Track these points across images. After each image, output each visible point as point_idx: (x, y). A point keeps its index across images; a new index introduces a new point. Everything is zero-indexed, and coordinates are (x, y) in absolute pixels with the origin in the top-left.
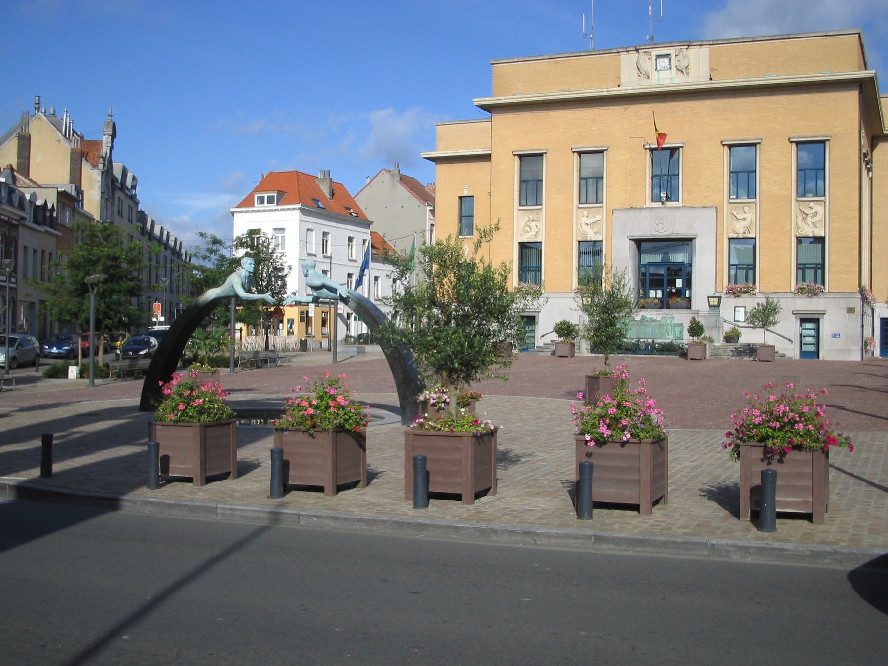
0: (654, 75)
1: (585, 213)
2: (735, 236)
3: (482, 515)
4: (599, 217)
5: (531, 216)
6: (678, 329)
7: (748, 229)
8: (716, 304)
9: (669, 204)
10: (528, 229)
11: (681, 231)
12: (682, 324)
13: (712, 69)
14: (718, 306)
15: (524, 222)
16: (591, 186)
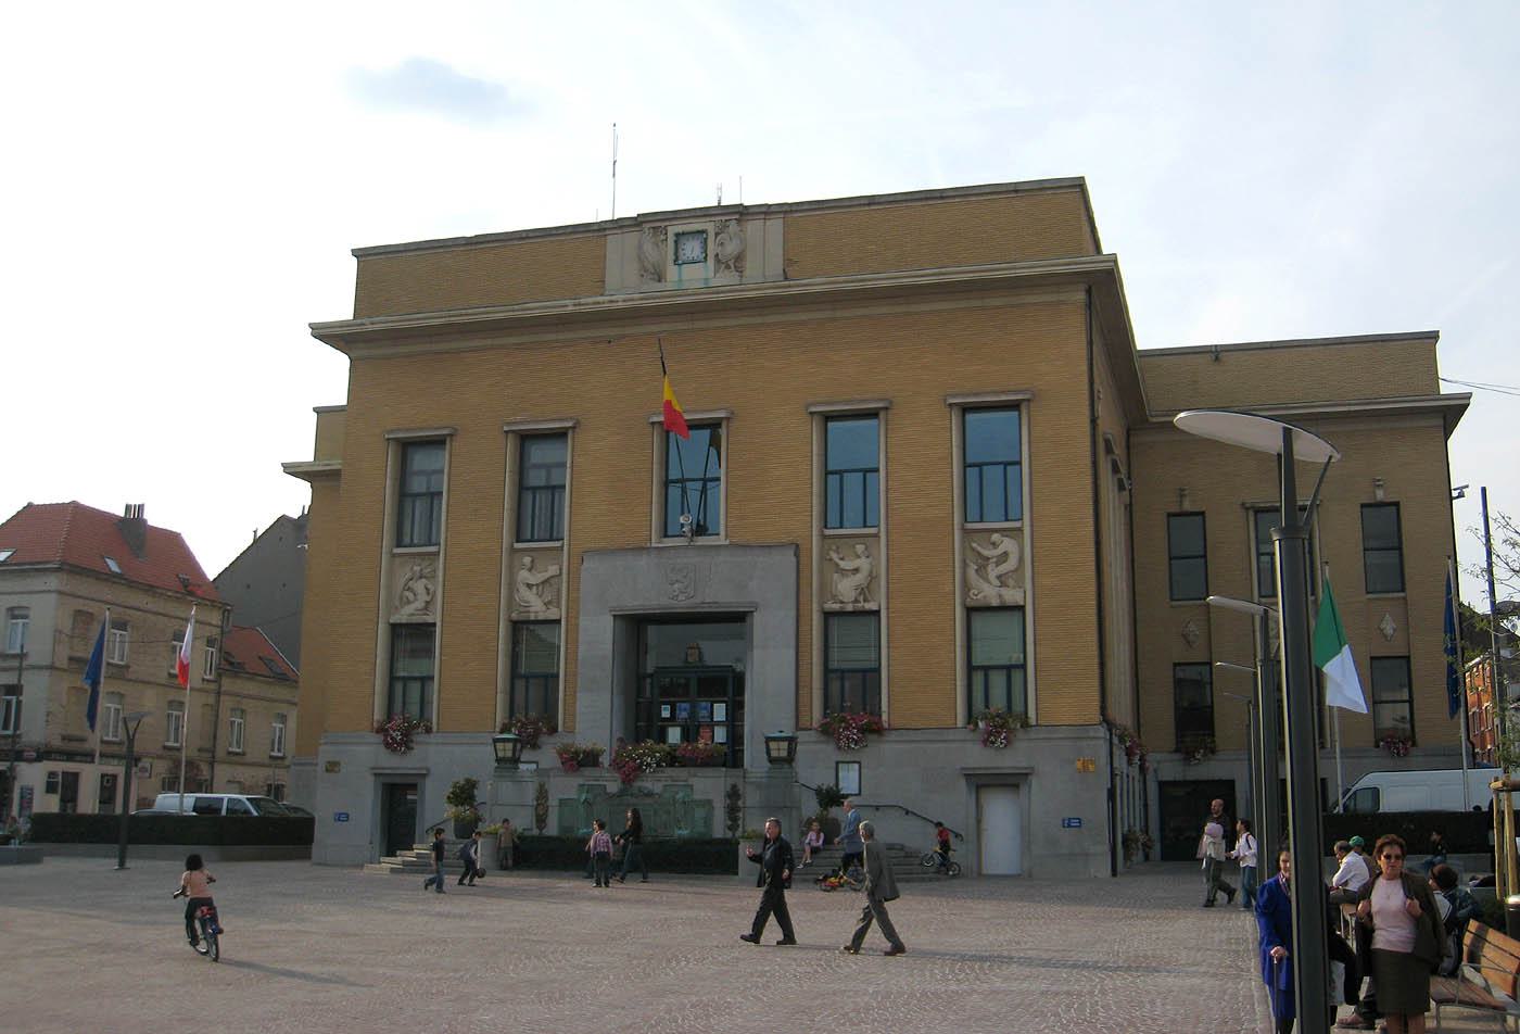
0: (672, 272)
1: (527, 560)
2: (836, 607)
3: (1415, 874)
4: (553, 570)
5: (417, 568)
6: (699, 813)
7: (865, 591)
8: (784, 754)
9: (701, 541)
10: (411, 596)
11: (718, 595)
12: (709, 802)
14: (790, 759)
15: (403, 581)
16: (535, 510)
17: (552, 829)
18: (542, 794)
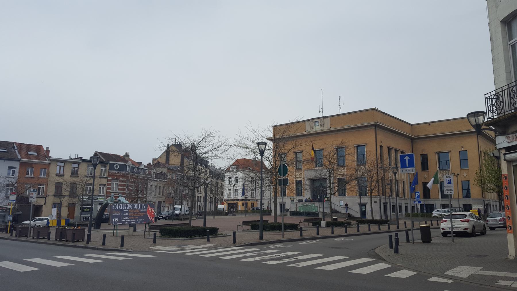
13: (331, 125)
17: (298, 211)
18: (297, 206)
